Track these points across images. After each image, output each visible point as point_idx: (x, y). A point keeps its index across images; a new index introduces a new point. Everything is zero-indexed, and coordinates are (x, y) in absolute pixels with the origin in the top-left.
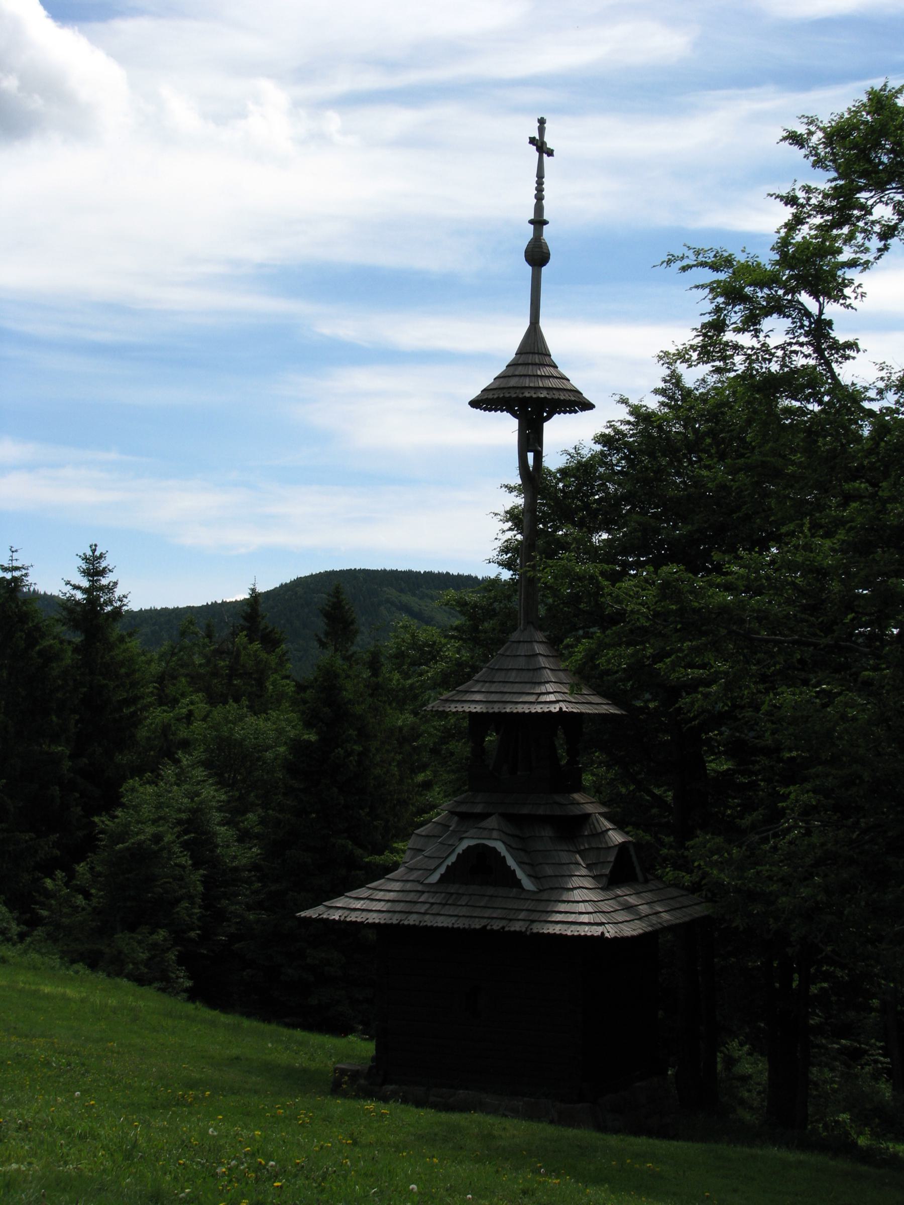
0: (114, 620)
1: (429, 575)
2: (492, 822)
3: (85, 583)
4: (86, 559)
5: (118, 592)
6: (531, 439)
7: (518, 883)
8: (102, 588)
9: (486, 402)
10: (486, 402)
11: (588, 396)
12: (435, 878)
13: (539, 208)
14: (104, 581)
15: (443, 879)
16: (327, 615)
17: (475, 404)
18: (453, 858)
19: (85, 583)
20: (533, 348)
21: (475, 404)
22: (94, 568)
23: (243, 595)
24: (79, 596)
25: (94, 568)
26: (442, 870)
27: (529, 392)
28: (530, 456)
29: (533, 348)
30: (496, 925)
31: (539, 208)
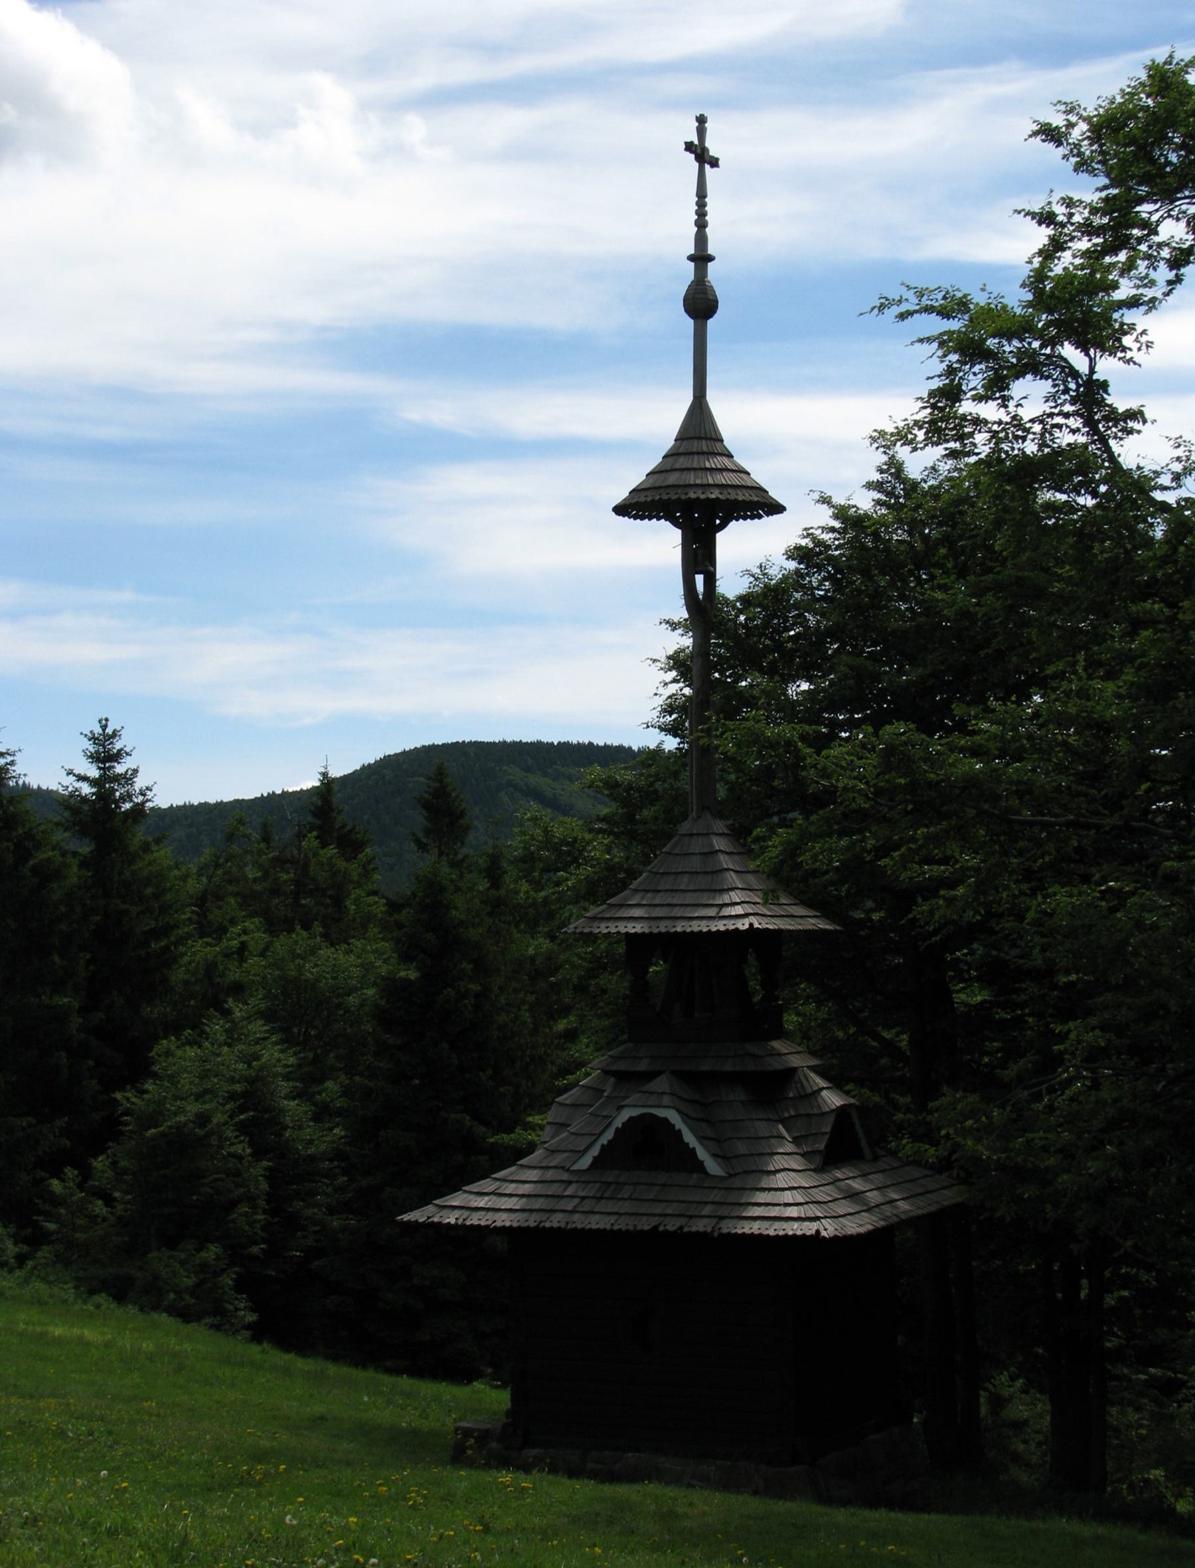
0: (135, 821)
1: (565, 747)
2: (661, 1084)
3: (93, 772)
4: (93, 738)
5: (140, 783)
6: (699, 556)
7: (700, 1167)
8: (117, 778)
9: (637, 506)
10: (637, 506)
11: (776, 494)
12: (585, 1162)
13: (701, 239)
14: (120, 769)
15: (597, 1163)
16: (427, 806)
17: (620, 510)
18: (609, 1135)
19: (93, 772)
20: (699, 430)
21: (620, 510)
22: (105, 750)
23: (310, 782)
24: (86, 789)
25: (105, 750)
26: (595, 1151)
27: (695, 492)
28: (699, 579)
29: (699, 430)
30: (671, 1225)
31: (701, 239)
